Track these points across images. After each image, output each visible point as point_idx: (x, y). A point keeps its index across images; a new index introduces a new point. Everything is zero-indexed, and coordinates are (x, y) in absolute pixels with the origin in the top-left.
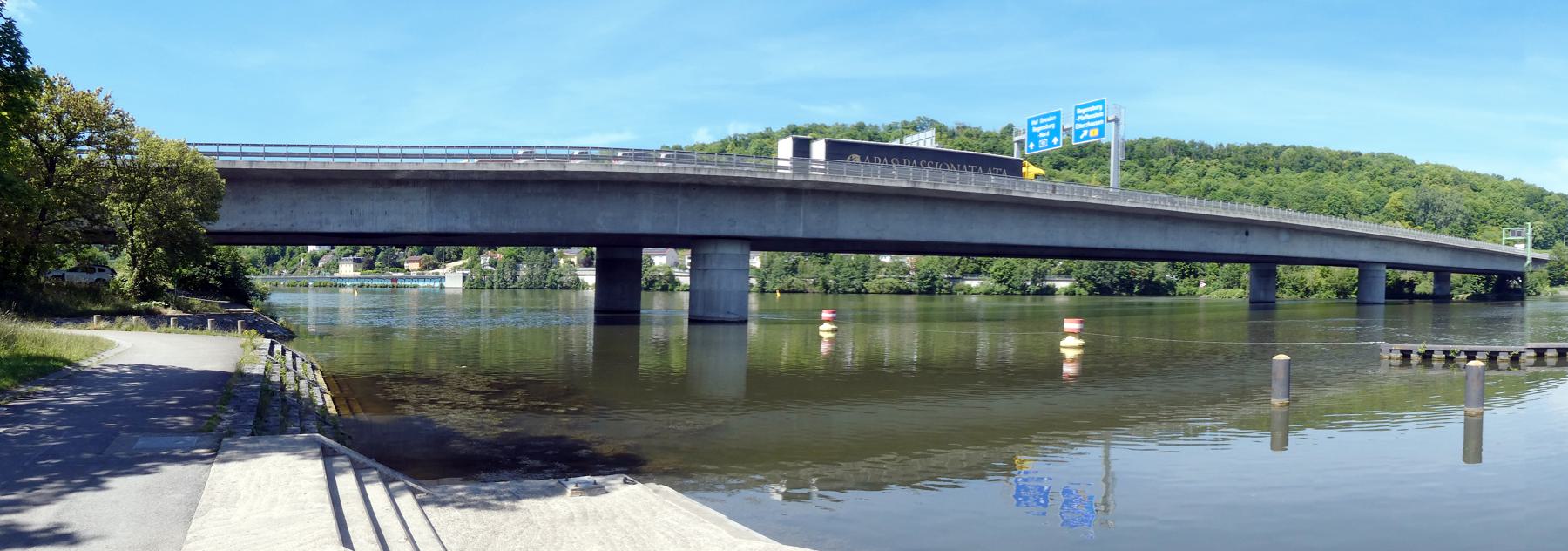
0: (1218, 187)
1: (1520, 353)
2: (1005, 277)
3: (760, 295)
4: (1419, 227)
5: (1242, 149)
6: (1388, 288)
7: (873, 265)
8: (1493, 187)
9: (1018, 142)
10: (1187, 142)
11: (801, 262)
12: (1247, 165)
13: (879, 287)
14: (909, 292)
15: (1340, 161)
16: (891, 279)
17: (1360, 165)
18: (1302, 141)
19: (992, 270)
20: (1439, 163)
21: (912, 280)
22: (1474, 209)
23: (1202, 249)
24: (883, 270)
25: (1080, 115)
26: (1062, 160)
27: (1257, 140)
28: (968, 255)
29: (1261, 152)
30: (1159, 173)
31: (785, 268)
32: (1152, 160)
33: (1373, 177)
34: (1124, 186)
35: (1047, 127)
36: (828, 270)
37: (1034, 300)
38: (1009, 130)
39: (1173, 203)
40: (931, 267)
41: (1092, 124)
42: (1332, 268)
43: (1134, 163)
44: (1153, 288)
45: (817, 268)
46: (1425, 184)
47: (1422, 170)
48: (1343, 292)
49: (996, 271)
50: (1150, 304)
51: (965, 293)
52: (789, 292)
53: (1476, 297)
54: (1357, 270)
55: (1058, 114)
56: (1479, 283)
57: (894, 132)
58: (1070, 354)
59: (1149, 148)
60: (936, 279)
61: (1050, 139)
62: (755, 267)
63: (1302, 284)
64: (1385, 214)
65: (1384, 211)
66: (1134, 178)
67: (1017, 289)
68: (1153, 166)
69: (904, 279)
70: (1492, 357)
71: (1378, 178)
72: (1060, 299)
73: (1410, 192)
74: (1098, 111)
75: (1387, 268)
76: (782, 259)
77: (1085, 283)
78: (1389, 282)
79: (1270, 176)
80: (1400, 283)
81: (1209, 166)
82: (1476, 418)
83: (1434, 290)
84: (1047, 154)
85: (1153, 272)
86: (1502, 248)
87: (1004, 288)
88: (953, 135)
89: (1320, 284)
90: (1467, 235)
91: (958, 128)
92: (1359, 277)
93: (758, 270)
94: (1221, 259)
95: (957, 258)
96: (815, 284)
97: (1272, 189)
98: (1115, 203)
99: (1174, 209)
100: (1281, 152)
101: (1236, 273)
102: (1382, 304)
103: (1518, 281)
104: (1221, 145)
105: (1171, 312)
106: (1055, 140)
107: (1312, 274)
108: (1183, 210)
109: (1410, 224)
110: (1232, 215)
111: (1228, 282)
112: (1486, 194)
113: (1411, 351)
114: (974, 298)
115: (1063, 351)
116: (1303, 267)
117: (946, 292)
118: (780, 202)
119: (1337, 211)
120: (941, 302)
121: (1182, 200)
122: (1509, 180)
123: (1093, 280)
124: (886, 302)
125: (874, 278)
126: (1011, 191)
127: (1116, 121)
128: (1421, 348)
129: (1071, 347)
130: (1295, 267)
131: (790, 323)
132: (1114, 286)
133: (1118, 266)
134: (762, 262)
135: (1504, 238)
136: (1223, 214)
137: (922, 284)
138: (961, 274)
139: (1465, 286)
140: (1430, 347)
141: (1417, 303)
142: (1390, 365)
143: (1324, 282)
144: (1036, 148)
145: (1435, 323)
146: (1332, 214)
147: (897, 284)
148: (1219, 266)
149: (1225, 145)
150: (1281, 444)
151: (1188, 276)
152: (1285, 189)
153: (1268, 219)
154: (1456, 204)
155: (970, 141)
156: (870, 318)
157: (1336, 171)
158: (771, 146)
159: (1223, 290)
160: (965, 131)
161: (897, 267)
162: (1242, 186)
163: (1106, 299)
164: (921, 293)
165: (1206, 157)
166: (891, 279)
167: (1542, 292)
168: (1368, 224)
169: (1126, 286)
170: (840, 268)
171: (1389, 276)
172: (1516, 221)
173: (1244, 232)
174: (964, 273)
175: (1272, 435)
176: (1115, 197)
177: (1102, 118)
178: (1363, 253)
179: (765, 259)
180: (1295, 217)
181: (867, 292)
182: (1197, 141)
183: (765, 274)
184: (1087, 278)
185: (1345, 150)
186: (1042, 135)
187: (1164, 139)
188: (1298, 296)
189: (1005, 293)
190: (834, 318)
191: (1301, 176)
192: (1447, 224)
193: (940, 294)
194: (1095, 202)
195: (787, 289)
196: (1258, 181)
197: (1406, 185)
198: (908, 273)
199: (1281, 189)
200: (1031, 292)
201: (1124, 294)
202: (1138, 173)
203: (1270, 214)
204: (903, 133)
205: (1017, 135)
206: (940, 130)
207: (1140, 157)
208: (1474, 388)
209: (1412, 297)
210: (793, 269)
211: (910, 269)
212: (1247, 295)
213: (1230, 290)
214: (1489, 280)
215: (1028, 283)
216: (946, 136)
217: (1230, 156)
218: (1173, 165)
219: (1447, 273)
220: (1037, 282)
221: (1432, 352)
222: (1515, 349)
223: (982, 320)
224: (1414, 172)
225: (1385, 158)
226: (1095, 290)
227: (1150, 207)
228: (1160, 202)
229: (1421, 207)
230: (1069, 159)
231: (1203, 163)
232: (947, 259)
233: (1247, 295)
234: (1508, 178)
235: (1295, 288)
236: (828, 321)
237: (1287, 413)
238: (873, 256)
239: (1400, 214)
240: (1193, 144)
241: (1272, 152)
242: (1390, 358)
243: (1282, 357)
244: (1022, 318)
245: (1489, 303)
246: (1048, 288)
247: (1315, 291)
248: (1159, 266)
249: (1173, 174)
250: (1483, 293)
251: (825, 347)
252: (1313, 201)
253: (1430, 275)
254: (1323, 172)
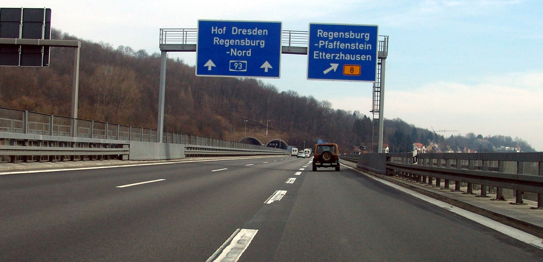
35: (247, 42)
41: (348, 57)
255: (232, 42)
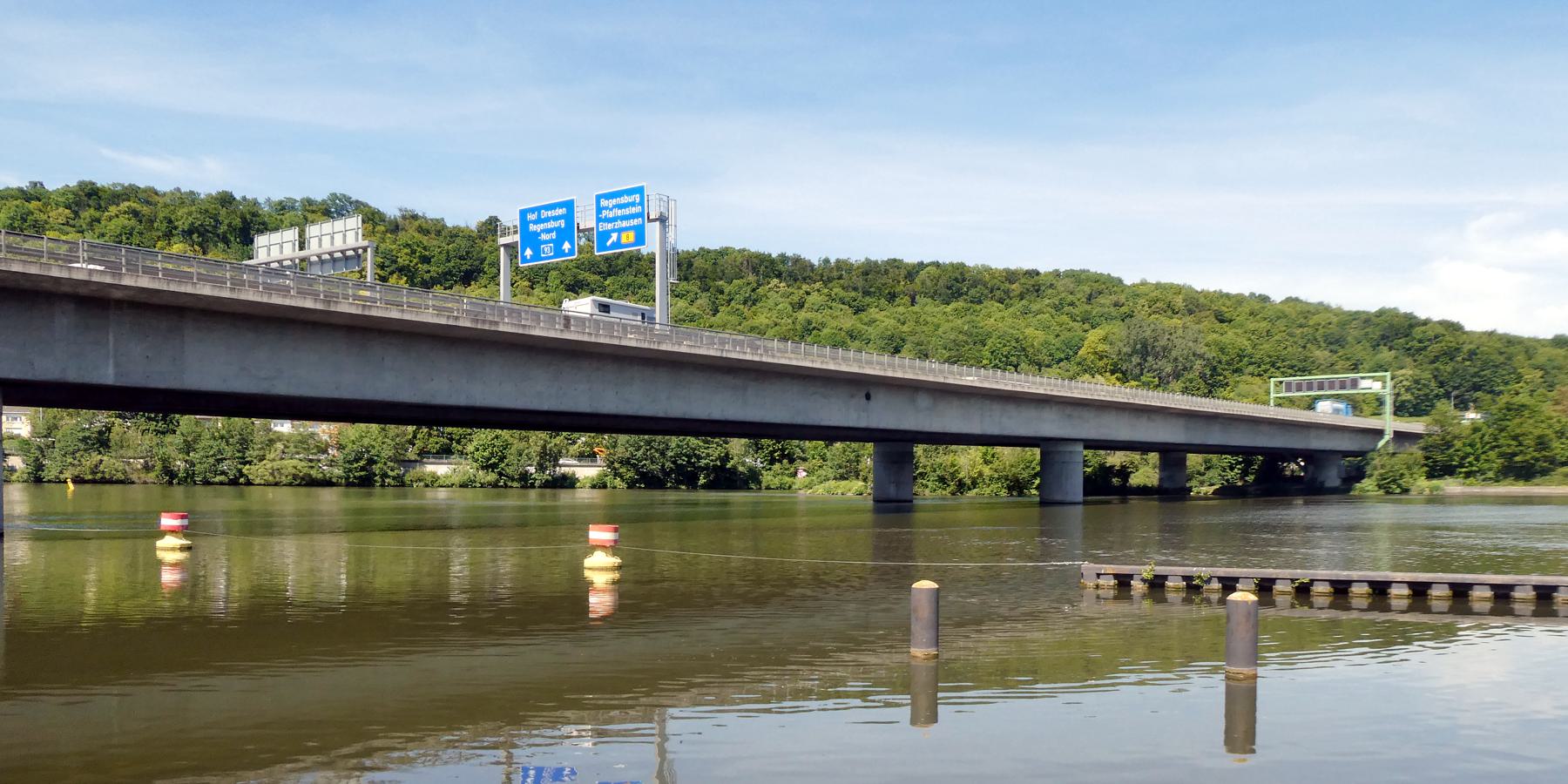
0: (823, 325)
1: (1312, 581)
2: (493, 460)
3: (32, 487)
4: (1134, 383)
5: (858, 268)
6: (1088, 480)
7: (259, 437)
8: (1251, 314)
9: (506, 246)
10: (774, 256)
11: (116, 429)
12: (866, 293)
13: (272, 474)
14: (327, 483)
15: (1007, 285)
16: (294, 462)
17: (1037, 290)
18: (948, 255)
19: (470, 448)
20: (1163, 281)
21: (332, 463)
22: (1222, 350)
23: (799, 420)
24: (279, 446)
25: (606, 208)
26: (581, 277)
27: (880, 255)
28: (430, 424)
29: (886, 272)
30: (733, 303)
31: (84, 440)
32: (721, 283)
33: (1058, 308)
34: (678, 321)
35: (552, 225)
36: (171, 444)
37: (542, 497)
38: (491, 227)
39: (755, 348)
40: (366, 442)
41: (625, 224)
42: (998, 449)
43: (693, 287)
44: (726, 478)
45: (149, 440)
46: (1141, 314)
47: (1136, 292)
48: (1016, 486)
49: (478, 450)
50: (725, 503)
51: (427, 486)
52: (94, 482)
53: (1227, 492)
54: (1037, 451)
55: (569, 205)
56: (1232, 469)
57: (289, 216)
58: (600, 579)
59: (714, 264)
60: (375, 462)
61: (558, 243)
62: (18, 436)
63: (953, 475)
64: (1080, 363)
65: (1078, 360)
66: (694, 310)
67: (513, 479)
68: (722, 292)
69: (319, 461)
70: (1265, 587)
71: (1066, 309)
72: (584, 495)
73: (1117, 329)
74: (633, 204)
75: (1086, 447)
76: (75, 422)
77: (621, 470)
78: (1089, 470)
79: (901, 309)
80: (1105, 471)
81: (808, 293)
82: (1244, 684)
83: (1161, 480)
84: (556, 267)
85: (727, 454)
86: (1271, 412)
87: (492, 477)
88: (395, 228)
89: (981, 474)
90: (1210, 392)
91: (404, 217)
92: (1042, 463)
93: (26, 442)
94: (830, 434)
95: (411, 429)
96: (147, 468)
97: (905, 328)
98: (664, 347)
99: (757, 359)
100: (918, 272)
101: (852, 456)
102: (1079, 503)
103: (1298, 464)
104: (827, 261)
105: (754, 515)
106: (566, 246)
107: (968, 459)
108: (770, 360)
109: (1118, 379)
110: (844, 368)
111: (841, 471)
112: (1241, 326)
113: (1131, 576)
114: (442, 494)
115: (587, 573)
116: (954, 447)
117: (392, 482)
118: (64, 320)
119: (1007, 363)
120: (382, 501)
121: (769, 344)
122: (1278, 301)
123: (634, 466)
124: (286, 501)
125: (262, 458)
126: (497, 323)
127: (662, 220)
128: (1147, 571)
129: (600, 569)
130: (941, 448)
131: (99, 536)
132: (667, 474)
133: (673, 445)
134: (34, 426)
135: (1273, 395)
136: (832, 367)
137: (350, 471)
138: (419, 455)
139: (1210, 474)
140: (1161, 570)
141: (1135, 501)
142: (1098, 597)
143: (987, 471)
144: (536, 257)
145: (1166, 529)
146: (996, 366)
147: (305, 470)
148: (827, 446)
149: (833, 261)
150: (927, 715)
151: (780, 461)
152: (925, 328)
153: (899, 375)
154: (1191, 344)
155: (425, 240)
156: (262, 525)
157: (1001, 301)
158: (45, 217)
159: (832, 483)
160: (417, 223)
161: (303, 442)
162: (859, 325)
163: (657, 495)
164: (349, 485)
165: (804, 279)
166: (294, 462)
167: (1413, 488)
168: (1053, 381)
169: (686, 475)
170: (195, 441)
171: (1082, 462)
172: (1292, 367)
173: (863, 394)
174: (424, 454)
175: (914, 704)
176: (663, 338)
177: (640, 215)
178: (1049, 425)
179: (40, 423)
180: (941, 371)
181: (249, 483)
182: (789, 254)
183: (40, 448)
184: (625, 462)
185: (1013, 267)
186: (544, 237)
187: (739, 251)
188: (946, 492)
189: (495, 485)
190: (185, 527)
191: (949, 309)
192: (1177, 375)
193: (383, 486)
194: (633, 344)
195: (90, 477)
196: (884, 318)
197: (1109, 318)
198: (325, 451)
199: (918, 329)
200: (537, 483)
201: (683, 487)
202: (699, 301)
203: (902, 367)
204: (306, 218)
205: (503, 235)
206: (372, 218)
207: (703, 278)
208: (1241, 634)
209: (1126, 492)
210: (102, 442)
211: (328, 445)
212: (869, 491)
213: (843, 483)
214: (1248, 463)
215: (532, 470)
216: (383, 228)
217: (840, 278)
218: (754, 290)
219: (1181, 454)
220: (546, 468)
221: (1165, 578)
222: (1304, 575)
223: (459, 528)
224: (1122, 298)
225: (1077, 277)
226: (637, 481)
227: (718, 354)
228: (735, 347)
229: (1135, 352)
230: (592, 278)
231: (800, 288)
232: (393, 429)
233: (869, 491)
234: (1277, 297)
235: (942, 480)
236: (173, 531)
237: (936, 669)
238: (257, 422)
239: (1101, 364)
240: (783, 258)
241: (903, 272)
242: (1097, 587)
243: (926, 584)
244: (521, 525)
245: (1250, 501)
246: (564, 477)
247: (974, 484)
248: (737, 446)
249: (754, 304)
250: (1240, 484)
251: (169, 577)
252: (967, 348)
253: (1154, 457)
254: (980, 302)
255: (542, 226)
